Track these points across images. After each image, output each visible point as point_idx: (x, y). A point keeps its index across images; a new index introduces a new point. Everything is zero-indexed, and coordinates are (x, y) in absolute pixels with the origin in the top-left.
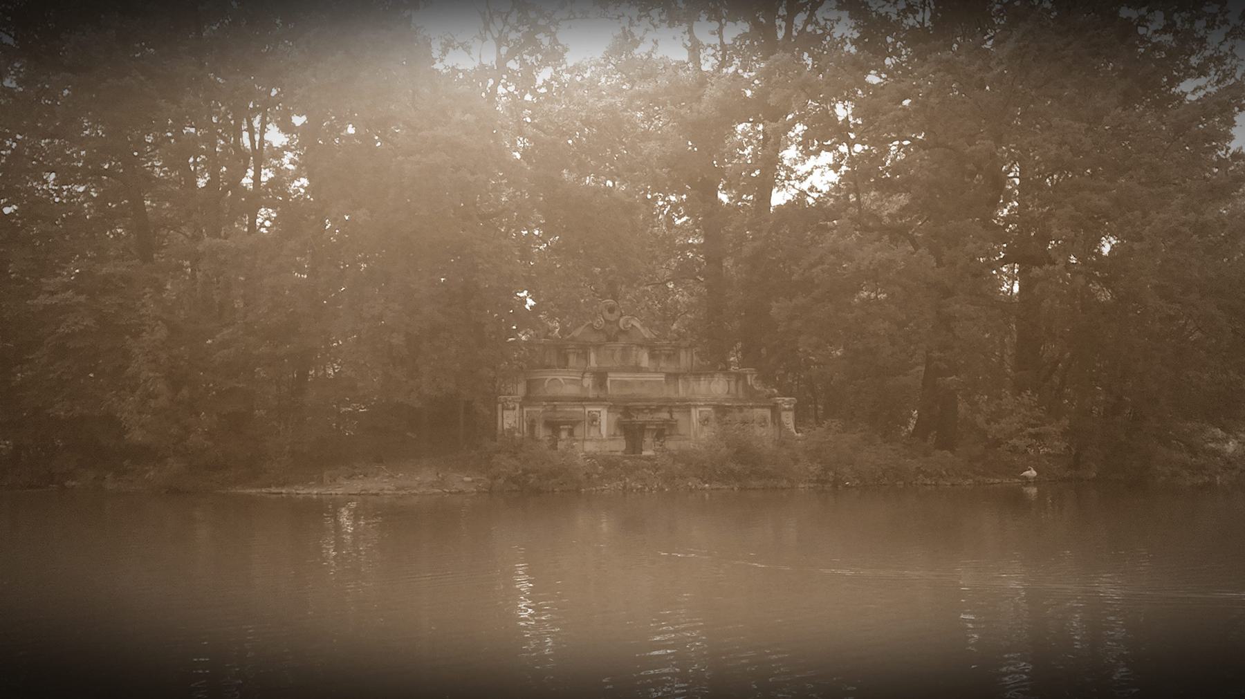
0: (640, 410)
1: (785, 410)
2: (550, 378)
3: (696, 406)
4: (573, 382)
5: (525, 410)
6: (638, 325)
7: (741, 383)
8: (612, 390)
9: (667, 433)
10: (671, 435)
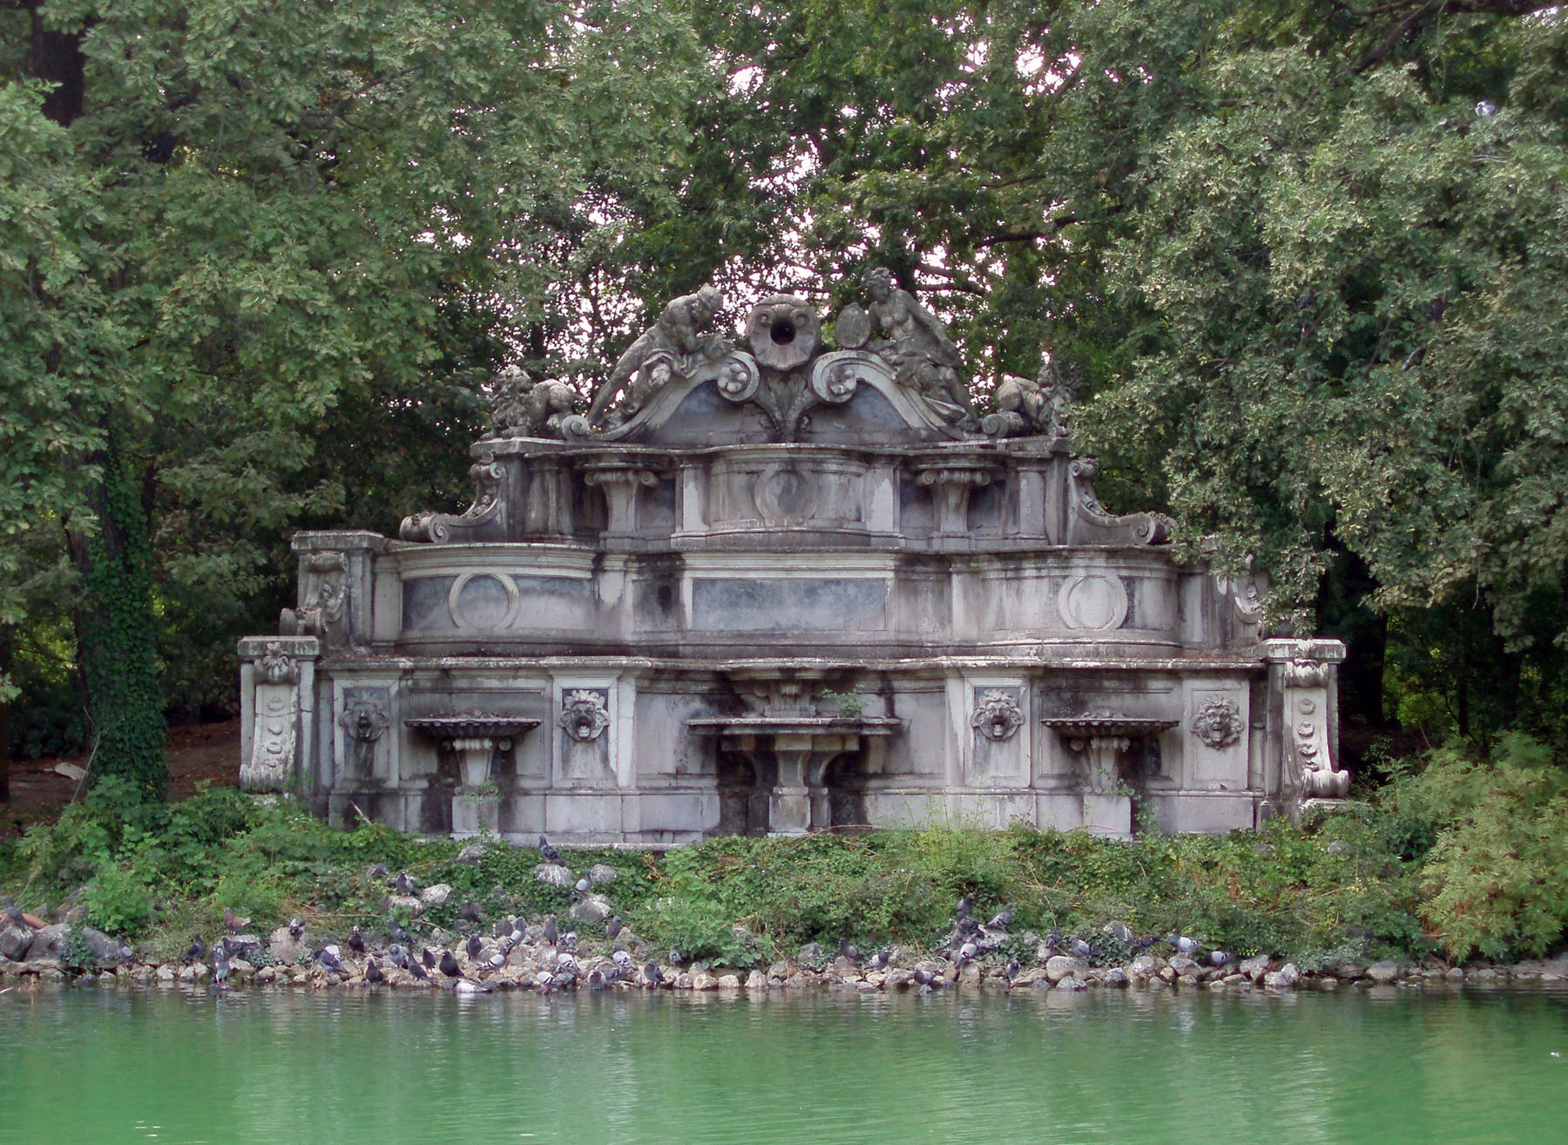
0: (770, 686)
1: (1294, 684)
2: (466, 573)
3: (961, 672)
4: (556, 586)
5: (340, 685)
6: (881, 381)
7: (1195, 587)
8: (700, 617)
9: (873, 765)
10: (885, 774)
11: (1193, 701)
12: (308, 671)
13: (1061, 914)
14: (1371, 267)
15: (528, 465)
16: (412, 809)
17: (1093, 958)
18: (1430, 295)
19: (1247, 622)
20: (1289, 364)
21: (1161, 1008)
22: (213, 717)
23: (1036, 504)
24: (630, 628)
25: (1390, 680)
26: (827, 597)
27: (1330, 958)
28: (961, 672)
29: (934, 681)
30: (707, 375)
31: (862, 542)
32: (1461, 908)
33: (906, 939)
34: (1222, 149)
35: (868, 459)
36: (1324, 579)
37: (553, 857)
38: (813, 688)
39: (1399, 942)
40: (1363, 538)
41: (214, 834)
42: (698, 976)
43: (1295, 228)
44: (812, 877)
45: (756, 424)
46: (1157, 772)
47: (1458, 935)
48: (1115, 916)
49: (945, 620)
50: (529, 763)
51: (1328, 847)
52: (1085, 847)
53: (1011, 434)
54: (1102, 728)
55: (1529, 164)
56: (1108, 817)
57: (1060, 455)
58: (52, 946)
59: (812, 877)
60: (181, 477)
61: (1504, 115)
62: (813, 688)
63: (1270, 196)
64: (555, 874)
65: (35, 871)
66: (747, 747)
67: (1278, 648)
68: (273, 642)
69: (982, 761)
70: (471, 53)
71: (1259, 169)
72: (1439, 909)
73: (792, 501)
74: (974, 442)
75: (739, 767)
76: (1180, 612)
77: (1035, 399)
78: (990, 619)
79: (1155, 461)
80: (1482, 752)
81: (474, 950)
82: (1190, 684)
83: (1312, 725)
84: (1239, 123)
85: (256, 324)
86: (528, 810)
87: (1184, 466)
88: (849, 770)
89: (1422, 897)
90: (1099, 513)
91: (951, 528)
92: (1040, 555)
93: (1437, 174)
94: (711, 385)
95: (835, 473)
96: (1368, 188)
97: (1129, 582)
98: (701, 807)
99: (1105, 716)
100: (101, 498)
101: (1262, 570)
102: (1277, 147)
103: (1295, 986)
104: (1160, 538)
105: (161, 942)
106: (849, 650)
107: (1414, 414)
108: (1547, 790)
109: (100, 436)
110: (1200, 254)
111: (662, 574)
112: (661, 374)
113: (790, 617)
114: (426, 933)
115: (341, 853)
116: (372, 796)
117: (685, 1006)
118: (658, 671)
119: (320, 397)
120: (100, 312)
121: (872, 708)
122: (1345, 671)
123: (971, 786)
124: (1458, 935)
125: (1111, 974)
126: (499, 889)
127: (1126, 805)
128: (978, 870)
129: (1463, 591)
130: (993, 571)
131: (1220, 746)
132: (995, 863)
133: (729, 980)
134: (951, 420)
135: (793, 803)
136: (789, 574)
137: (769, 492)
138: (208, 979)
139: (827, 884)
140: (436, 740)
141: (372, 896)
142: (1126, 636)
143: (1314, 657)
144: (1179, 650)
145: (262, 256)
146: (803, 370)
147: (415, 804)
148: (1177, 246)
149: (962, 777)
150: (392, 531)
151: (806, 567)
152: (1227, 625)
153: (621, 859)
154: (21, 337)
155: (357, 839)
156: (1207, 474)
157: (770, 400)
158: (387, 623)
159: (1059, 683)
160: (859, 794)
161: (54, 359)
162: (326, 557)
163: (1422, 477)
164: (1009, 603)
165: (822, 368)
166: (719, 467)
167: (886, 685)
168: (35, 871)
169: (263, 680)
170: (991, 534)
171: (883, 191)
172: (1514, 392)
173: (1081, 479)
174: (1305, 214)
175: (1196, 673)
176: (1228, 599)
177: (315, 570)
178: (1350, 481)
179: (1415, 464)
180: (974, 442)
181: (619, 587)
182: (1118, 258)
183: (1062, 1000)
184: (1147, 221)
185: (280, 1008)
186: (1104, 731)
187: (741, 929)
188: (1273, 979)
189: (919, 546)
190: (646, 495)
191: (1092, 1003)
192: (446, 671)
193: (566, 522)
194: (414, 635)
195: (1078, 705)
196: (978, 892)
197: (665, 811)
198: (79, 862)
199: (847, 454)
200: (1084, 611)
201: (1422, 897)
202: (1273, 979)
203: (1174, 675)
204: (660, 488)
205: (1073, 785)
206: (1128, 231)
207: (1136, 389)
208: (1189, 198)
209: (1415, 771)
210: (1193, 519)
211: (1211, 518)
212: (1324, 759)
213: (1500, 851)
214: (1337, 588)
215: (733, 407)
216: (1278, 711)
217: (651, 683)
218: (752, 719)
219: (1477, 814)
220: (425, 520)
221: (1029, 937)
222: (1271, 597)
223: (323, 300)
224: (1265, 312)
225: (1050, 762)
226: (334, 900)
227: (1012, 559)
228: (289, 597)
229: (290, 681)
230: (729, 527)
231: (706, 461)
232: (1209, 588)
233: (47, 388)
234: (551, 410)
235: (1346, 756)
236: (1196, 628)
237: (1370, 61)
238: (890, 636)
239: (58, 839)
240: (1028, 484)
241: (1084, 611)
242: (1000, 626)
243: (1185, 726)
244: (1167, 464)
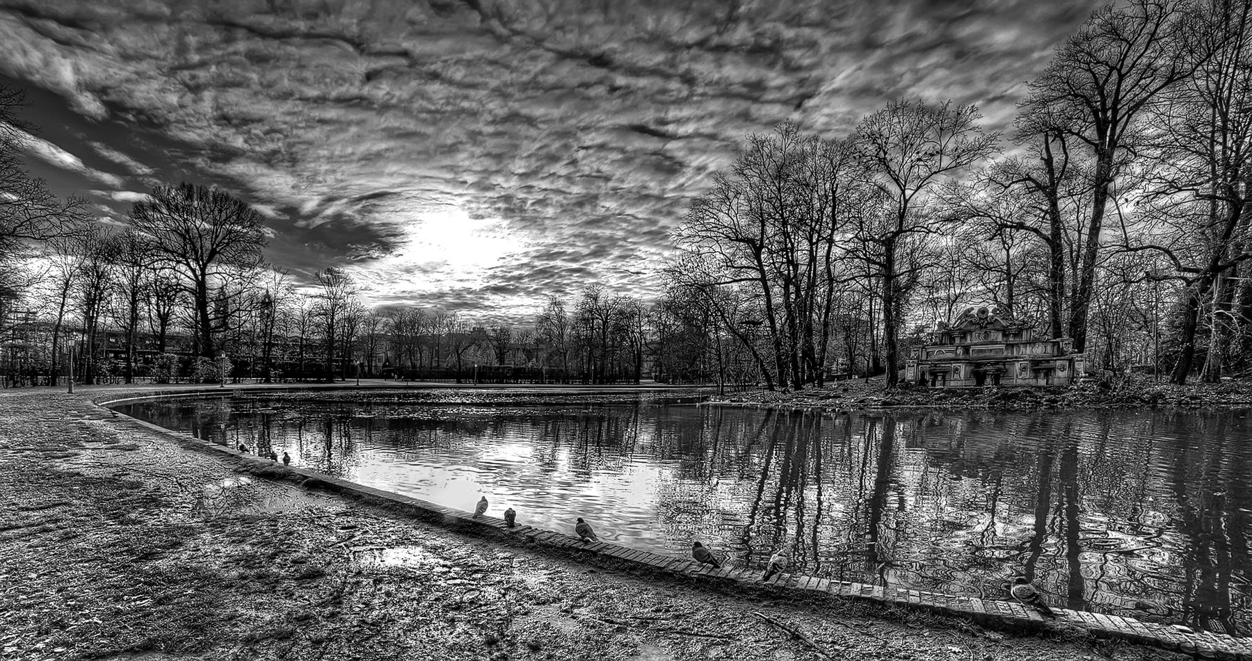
95: (1055, 314)
98: (972, 383)
109: (937, 66)
118: (498, 417)
151: (990, 347)
158: (924, 358)
181: (960, 351)
205: (1036, 377)
240: (1024, 333)
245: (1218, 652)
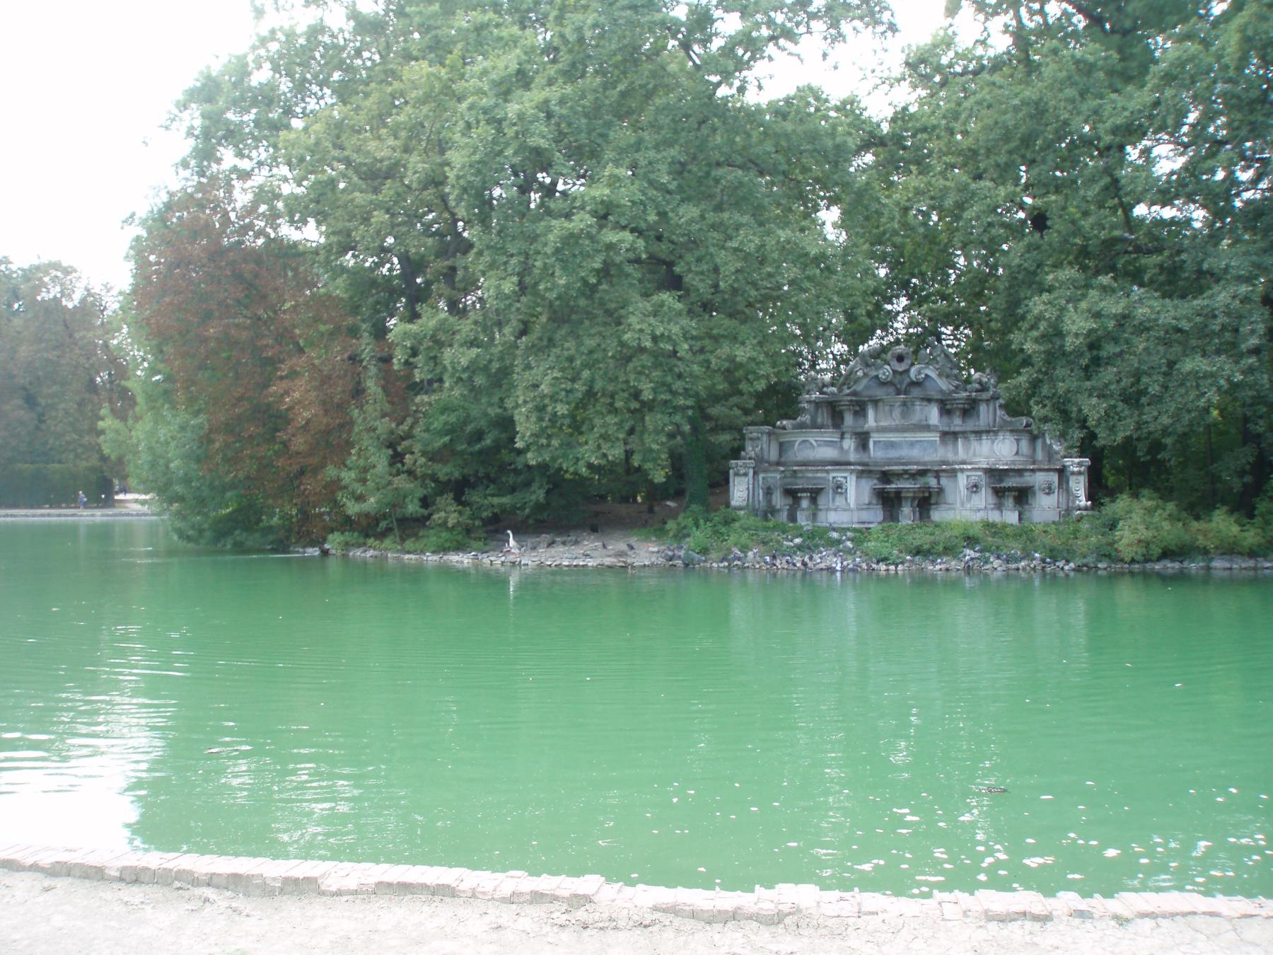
1: (1073, 473)
2: (800, 439)
3: (962, 470)
5: (761, 476)
6: (933, 374)
7: (1039, 443)
9: (933, 501)
10: (937, 503)
11: (1040, 479)
12: (751, 472)
13: (998, 548)
14: (1099, 339)
15: (817, 404)
16: (784, 516)
17: (1008, 562)
18: (1118, 350)
19: (1057, 453)
20: (1072, 371)
21: (1031, 579)
22: (721, 483)
23: (985, 415)
24: (852, 457)
25: (1105, 472)
26: (918, 446)
27: (1085, 561)
28: (962, 470)
29: (953, 473)
30: (875, 373)
31: (927, 428)
32: (1128, 545)
33: (947, 555)
34: (1050, 303)
35: (929, 400)
36: (1083, 439)
37: (834, 530)
38: (914, 476)
39: (1108, 556)
40: (1096, 426)
41: (728, 522)
42: (883, 567)
43: (1074, 328)
44: (917, 536)
45: (891, 390)
46: (1027, 503)
47: (1127, 553)
48: (1016, 549)
49: (956, 453)
50: (822, 501)
51: (1085, 526)
52: (1005, 526)
53: (977, 391)
54: (1008, 488)
55: (1149, 307)
56: (1011, 517)
57: (995, 398)
58: (679, 557)
59: (917, 536)
60: (715, 411)
61: (1142, 290)
62: (914, 476)
63: (1066, 319)
64: (835, 535)
65: (671, 534)
66: (892, 495)
67: (1068, 461)
68: (740, 462)
69: (969, 499)
70: (809, 278)
71: (1062, 309)
72: (1121, 546)
73: (904, 415)
74: (964, 394)
75: (889, 502)
76: (1034, 450)
77: (985, 380)
78: (971, 452)
79: (1027, 402)
80: (1136, 496)
81: (811, 558)
82: (1038, 474)
83: (1079, 488)
84: (1055, 294)
85: (741, 365)
86: (821, 516)
87: (1037, 403)
88: (926, 502)
89: (1115, 542)
90: (1007, 417)
91: (957, 423)
92: (988, 432)
93: (1120, 311)
94: (877, 377)
96: (1097, 315)
97: (1018, 441)
98: (875, 515)
99: (1010, 484)
100: (691, 420)
101: (1063, 436)
102: (1068, 302)
103: (1073, 570)
104: (1028, 425)
105: (713, 555)
106: (924, 464)
107: (1112, 387)
108: (1157, 507)
110: (1043, 336)
111: (863, 440)
112: (860, 374)
113: (904, 453)
114: (795, 553)
115: (766, 529)
116: (771, 511)
117: (878, 575)
119: (761, 386)
120: (693, 363)
121: (932, 482)
122: (1089, 468)
123: (965, 507)
124: (1127, 553)
125: (1014, 566)
126: (816, 539)
127: (1017, 513)
128: (971, 533)
129: (1128, 439)
130: (972, 437)
131: (1048, 494)
132: (976, 531)
133: (892, 567)
134: (957, 387)
135: (907, 513)
136: (906, 439)
137: (897, 412)
138: (729, 567)
139: (921, 538)
140: (792, 493)
141: (778, 542)
142: (1016, 458)
143: (1080, 464)
144: (1034, 463)
145: (743, 343)
146: (907, 371)
147: (785, 514)
148: (1035, 333)
149: (962, 504)
150: (774, 426)
151: (910, 437)
152: (1050, 454)
153: (855, 530)
154: (671, 370)
155: (771, 524)
156: (1045, 406)
157: (896, 381)
158: (774, 455)
159: (994, 474)
160: (928, 510)
161: (680, 376)
162: (755, 435)
163: (1115, 407)
164: (977, 448)
165: (913, 370)
166: (880, 404)
167: (937, 474)
168: (671, 534)
169: (737, 474)
170: (970, 425)
171: (932, 310)
172: (1145, 380)
173: (1001, 406)
174: (1077, 324)
175: (1040, 470)
176: (1051, 445)
177: (751, 439)
178: (1093, 408)
179: (1112, 403)
180: (964, 394)
181: (849, 444)
182: (1015, 337)
183: (999, 574)
184: (1025, 325)
185: (750, 576)
186: (1010, 489)
187: (895, 552)
188: (1066, 568)
189: (946, 429)
190: (856, 413)
191: (1008, 576)
192: (795, 472)
193: (830, 422)
194: (783, 459)
195: (1001, 481)
196: (971, 541)
197: (865, 516)
198: (685, 531)
199: (923, 399)
200: (1002, 450)
201: (1115, 542)
202: (1066, 568)
203: (1033, 471)
204: (860, 411)
205: (999, 507)
206: (1019, 329)
207: (1022, 379)
208: (1039, 318)
209: (1113, 501)
210: (1040, 420)
211: (1045, 420)
212: (1083, 498)
213: (1141, 527)
214: (1087, 441)
215: (884, 384)
216: (1068, 483)
217: (861, 475)
218: (893, 486)
219: (1133, 515)
220: (785, 422)
221: (987, 554)
222: (1066, 444)
223: (762, 358)
224: (1064, 354)
225: (992, 499)
226: (765, 543)
227: (978, 433)
228: (742, 448)
229: (746, 475)
230: (884, 424)
231: (876, 402)
232: (1044, 442)
233: (678, 385)
234: (824, 386)
235: (1090, 497)
236: (1040, 455)
237: (1098, 272)
238: (938, 459)
239: (678, 524)
240: (983, 408)
241: (1002, 450)
242: (975, 455)
243: (1037, 487)
244: (1032, 403)
245: (951, 891)
